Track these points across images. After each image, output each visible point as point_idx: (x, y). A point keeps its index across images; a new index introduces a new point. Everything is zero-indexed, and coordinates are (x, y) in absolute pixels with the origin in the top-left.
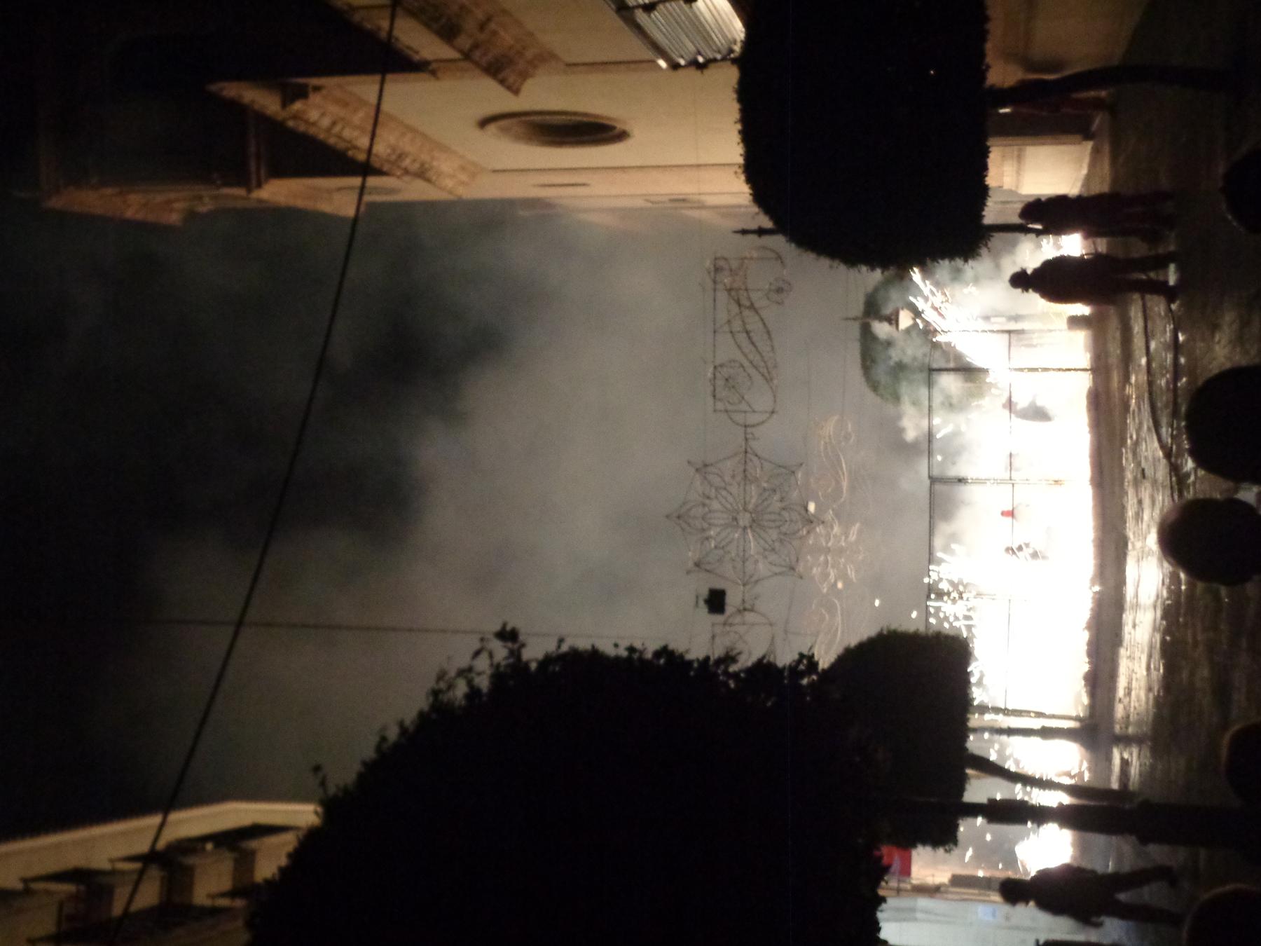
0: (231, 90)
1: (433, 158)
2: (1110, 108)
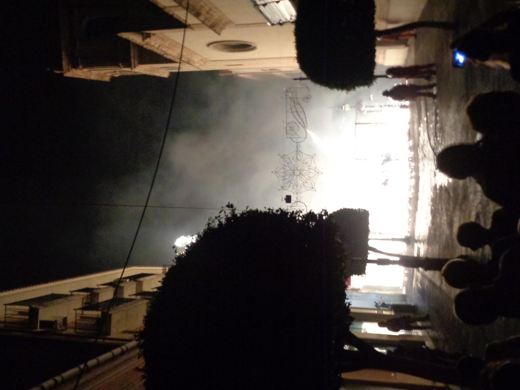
0: (125, 35)
1: (192, 57)
2: (415, 36)
